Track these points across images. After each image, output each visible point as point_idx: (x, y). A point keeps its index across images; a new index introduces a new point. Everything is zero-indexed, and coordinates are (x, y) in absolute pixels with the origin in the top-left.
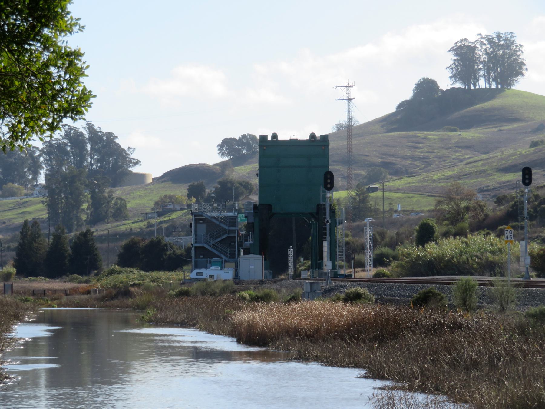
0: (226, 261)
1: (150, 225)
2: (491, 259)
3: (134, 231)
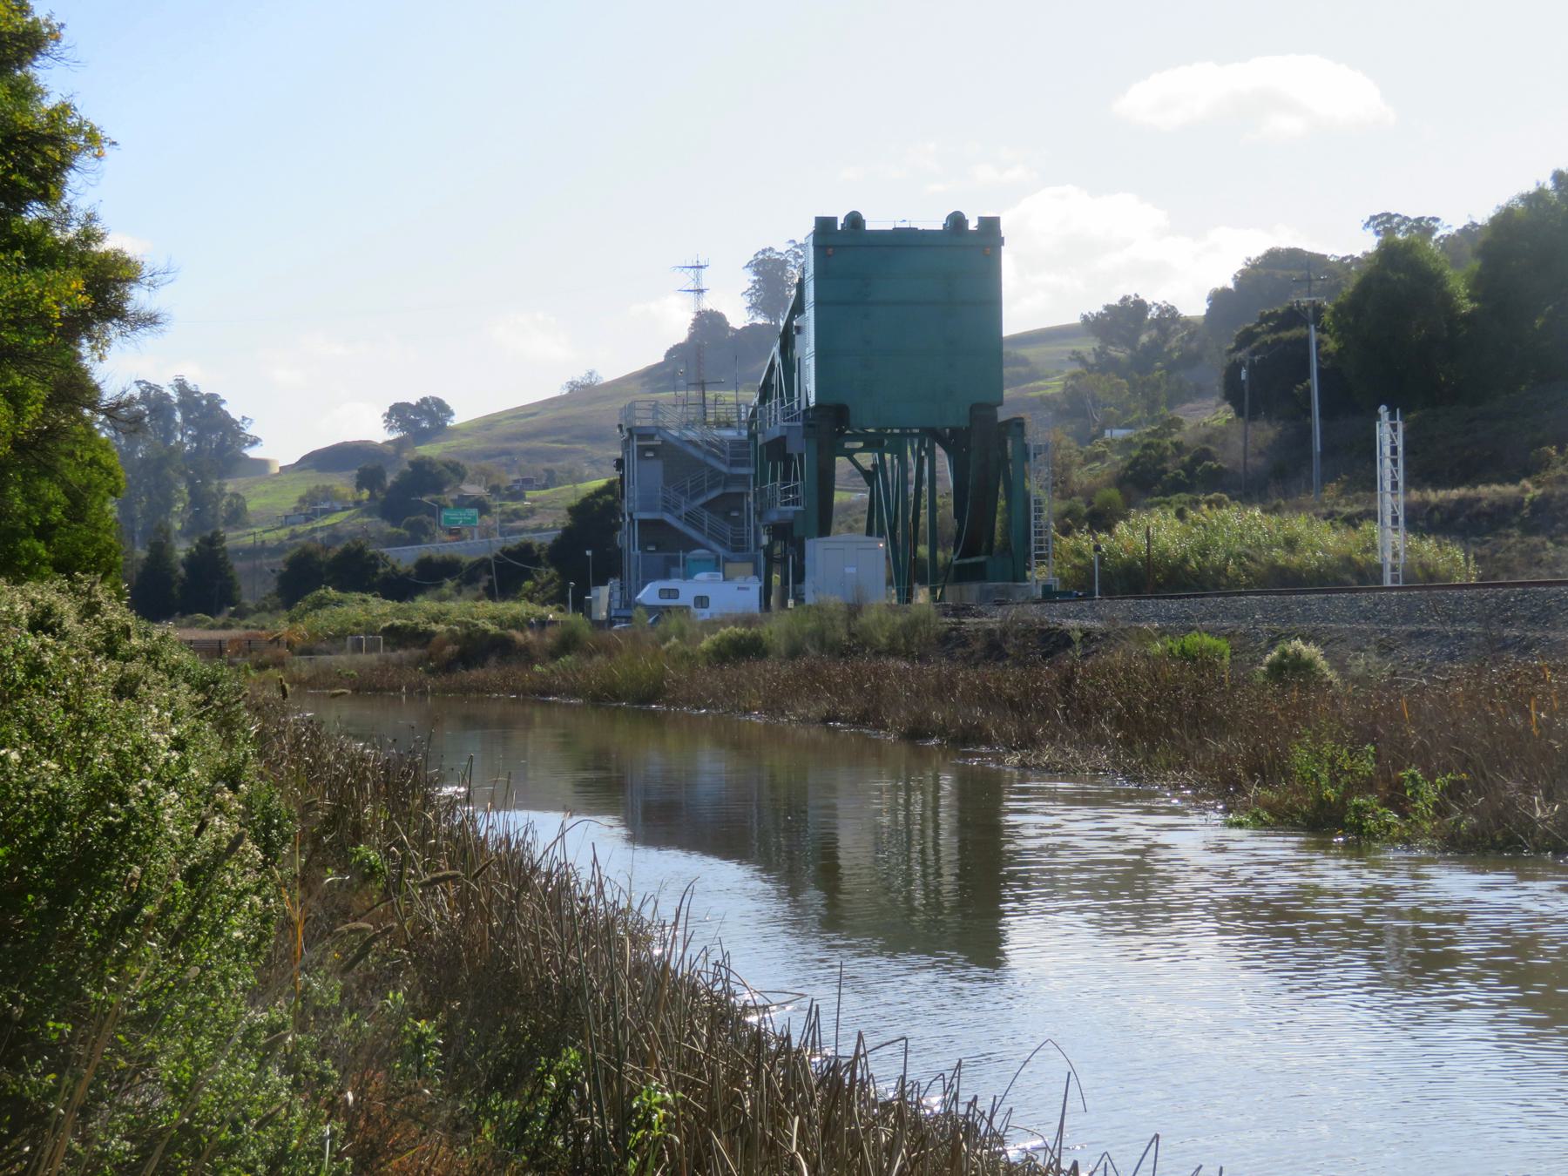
0: (727, 560)
1: (294, 536)
2: (1281, 562)
3: (268, 545)
